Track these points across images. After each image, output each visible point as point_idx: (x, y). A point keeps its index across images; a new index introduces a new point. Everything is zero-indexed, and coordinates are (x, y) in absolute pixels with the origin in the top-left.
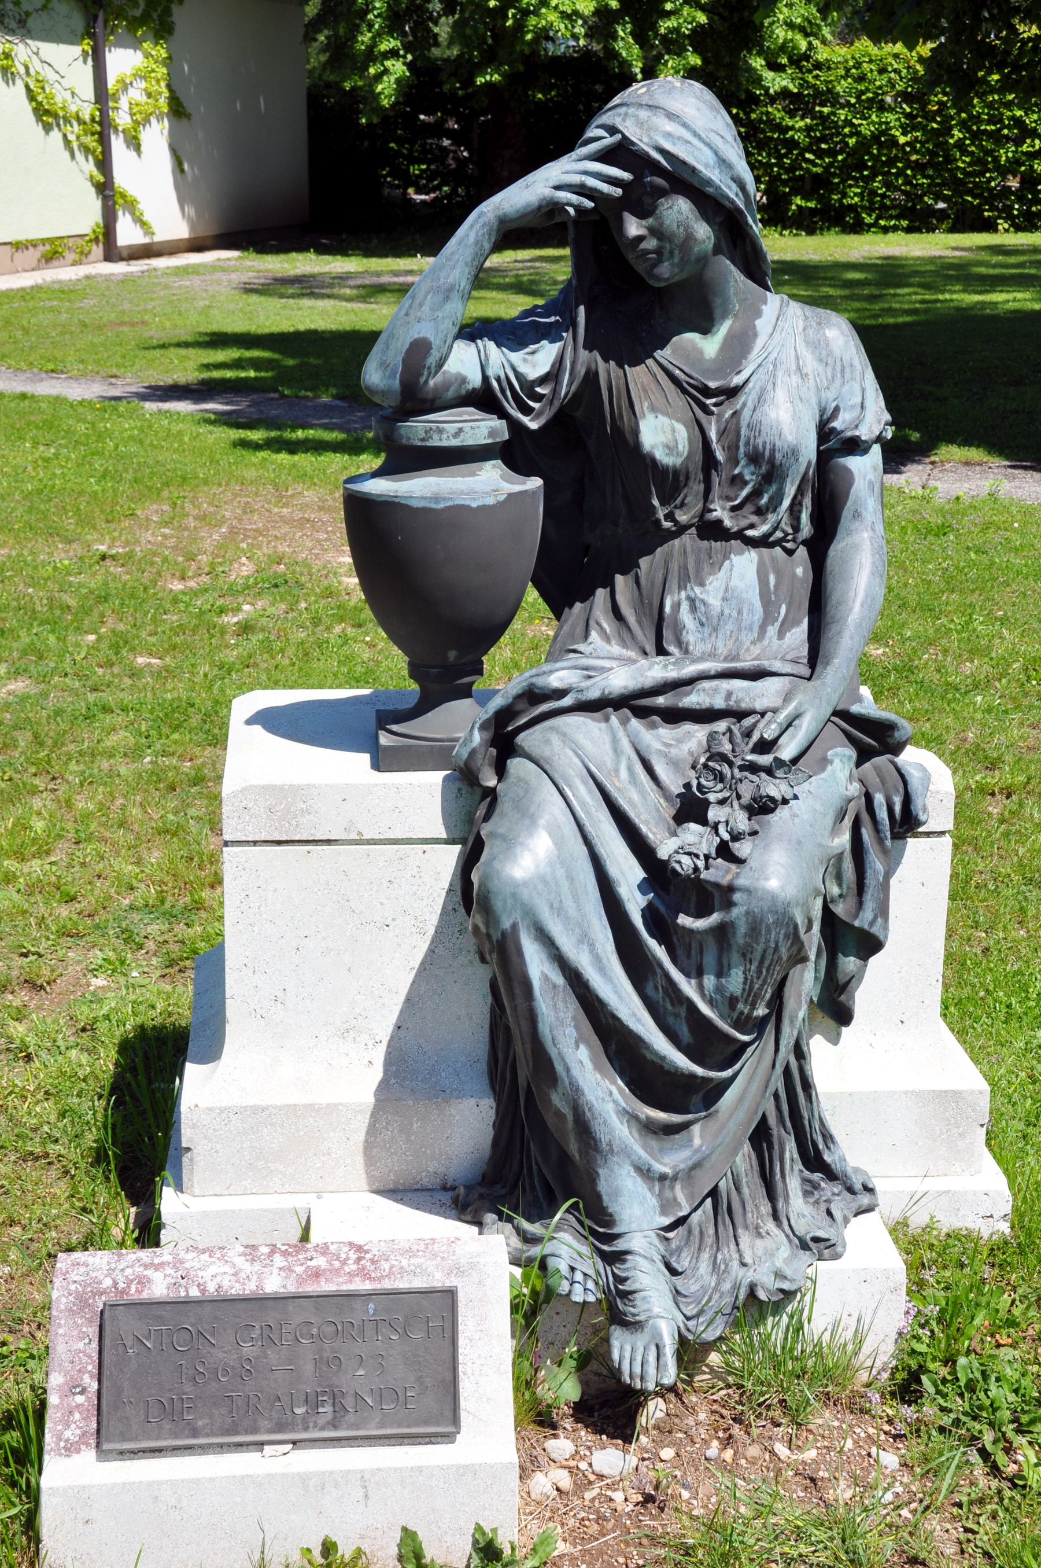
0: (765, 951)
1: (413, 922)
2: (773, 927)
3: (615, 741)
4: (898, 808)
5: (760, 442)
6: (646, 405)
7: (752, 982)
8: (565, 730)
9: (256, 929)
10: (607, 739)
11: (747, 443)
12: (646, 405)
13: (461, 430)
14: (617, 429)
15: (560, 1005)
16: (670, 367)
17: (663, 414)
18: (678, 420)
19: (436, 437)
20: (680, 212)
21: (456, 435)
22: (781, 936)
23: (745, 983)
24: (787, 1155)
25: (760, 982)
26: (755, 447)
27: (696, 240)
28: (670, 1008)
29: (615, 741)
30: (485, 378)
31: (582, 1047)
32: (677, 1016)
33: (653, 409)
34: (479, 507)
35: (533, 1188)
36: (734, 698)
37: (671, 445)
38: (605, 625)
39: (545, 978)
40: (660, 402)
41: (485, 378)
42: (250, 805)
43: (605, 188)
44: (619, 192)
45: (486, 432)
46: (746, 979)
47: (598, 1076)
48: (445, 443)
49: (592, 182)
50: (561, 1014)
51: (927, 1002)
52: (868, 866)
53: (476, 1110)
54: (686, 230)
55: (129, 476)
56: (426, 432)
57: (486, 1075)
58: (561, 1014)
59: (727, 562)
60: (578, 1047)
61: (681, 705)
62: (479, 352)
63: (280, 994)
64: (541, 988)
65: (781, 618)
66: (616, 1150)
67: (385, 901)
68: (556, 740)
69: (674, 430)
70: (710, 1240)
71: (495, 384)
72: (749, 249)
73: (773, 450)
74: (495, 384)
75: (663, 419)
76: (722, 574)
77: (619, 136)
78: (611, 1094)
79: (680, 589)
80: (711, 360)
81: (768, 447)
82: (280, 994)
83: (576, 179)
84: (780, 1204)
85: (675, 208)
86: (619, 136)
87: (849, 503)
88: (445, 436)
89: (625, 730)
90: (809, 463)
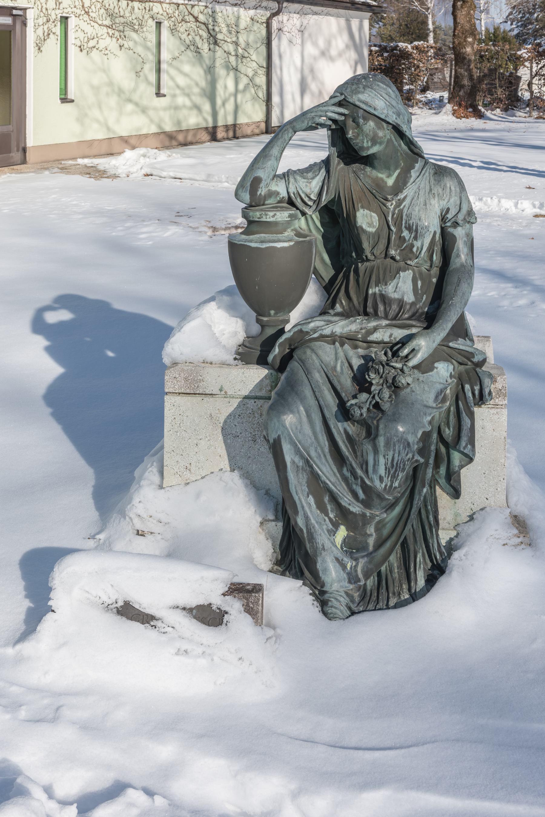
0: (394, 455)
1: (250, 435)
2: (397, 443)
3: (336, 354)
4: (477, 392)
5: (411, 222)
6: (360, 205)
7: (389, 469)
8: (314, 348)
9: (178, 434)
10: (333, 352)
11: (406, 223)
12: (360, 205)
13: (275, 214)
15: (301, 475)
16: (371, 190)
17: (367, 209)
18: (374, 212)
19: (264, 217)
20: (370, 126)
21: (273, 216)
22: (401, 448)
23: (386, 470)
24: (418, 560)
25: (394, 469)
26: (409, 225)
27: (378, 137)
28: (353, 480)
29: (336, 354)
31: (310, 496)
32: (357, 484)
33: (363, 207)
34: (281, 247)
35: (295, 568)
36: (393, 336)
37: (370, 223)
38: (343, 302)
39: (293, 462)
42: (177, 376)
44: (343, 118)
45: (287, 215)
46: (386, 468)
47: (319, 512)
48: (268, 220)
50: (301, 480)
51: (499, 489)
52: (462, 420)
53: (276, 528)
54: (373, 133)
56: (260, 215)
58: (301, 480)
59: (398, 275)
60: (308, 496)
61: (368, 339)
62: (286, 181)
63: (188, 466)
64: (291, 466)
65: (423, 301)
66: (326, 548)
67: (237, 424)
68: (309, 352)
69: (371, 216)
70: (374, 598)
71: (292, 195)
72: (408, 140)
75: (366, 212)
76: (395, 281)
78: (325, 520)
79: (376, 286)
82: (188, 466)
84: (413, 584)
85: (368, 124)
86: (343, 97)
87: (455, 251)
88: (268, 217)
89: (342, 349)
90: (435, 233)
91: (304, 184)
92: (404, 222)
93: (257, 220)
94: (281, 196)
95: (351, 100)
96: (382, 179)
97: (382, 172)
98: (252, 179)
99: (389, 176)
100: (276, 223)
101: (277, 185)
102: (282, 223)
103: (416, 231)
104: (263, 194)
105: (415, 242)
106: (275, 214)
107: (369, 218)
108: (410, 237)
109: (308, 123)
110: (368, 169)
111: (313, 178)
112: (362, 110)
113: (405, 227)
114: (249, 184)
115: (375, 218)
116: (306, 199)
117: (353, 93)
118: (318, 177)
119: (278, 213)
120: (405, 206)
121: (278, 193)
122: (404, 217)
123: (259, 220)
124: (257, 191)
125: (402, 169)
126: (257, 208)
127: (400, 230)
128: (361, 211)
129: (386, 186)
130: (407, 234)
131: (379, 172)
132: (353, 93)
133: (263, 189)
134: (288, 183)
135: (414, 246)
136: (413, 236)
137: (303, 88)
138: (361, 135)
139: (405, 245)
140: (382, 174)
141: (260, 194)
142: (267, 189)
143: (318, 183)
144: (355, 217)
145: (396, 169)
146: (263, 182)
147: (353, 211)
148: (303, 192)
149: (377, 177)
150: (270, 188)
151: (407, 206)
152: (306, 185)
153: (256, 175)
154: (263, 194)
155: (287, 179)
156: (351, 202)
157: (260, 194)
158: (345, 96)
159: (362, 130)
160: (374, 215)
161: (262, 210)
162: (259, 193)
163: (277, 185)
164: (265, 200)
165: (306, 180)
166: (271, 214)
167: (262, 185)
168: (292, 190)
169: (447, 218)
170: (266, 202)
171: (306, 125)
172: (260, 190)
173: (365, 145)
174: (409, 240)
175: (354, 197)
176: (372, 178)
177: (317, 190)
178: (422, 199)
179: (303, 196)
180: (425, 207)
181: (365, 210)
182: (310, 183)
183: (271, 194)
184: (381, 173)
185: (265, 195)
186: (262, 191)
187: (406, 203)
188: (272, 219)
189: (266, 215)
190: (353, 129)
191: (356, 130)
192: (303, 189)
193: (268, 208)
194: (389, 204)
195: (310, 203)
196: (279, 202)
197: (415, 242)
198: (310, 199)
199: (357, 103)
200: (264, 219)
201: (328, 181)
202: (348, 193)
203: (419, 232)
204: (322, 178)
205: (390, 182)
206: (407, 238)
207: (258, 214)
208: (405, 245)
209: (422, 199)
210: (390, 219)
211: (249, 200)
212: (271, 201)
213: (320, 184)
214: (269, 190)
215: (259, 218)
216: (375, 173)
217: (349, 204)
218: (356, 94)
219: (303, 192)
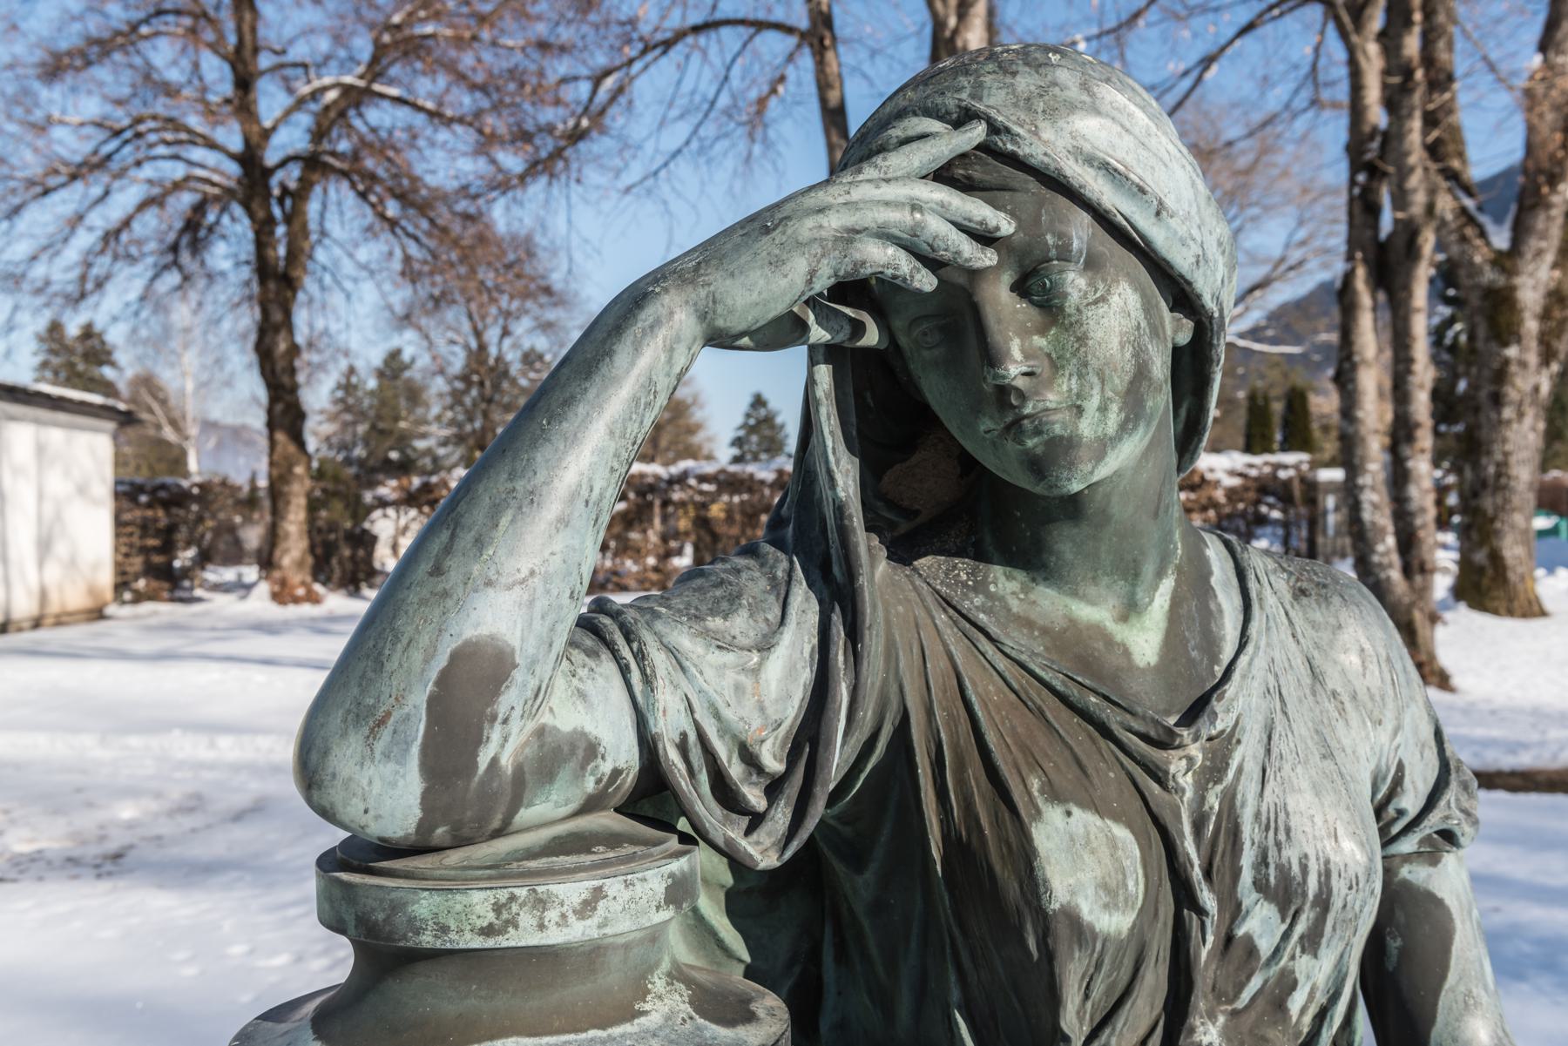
5: (1291, 855)
6: (1035, 784)
11: (1262, 861)
12: (1035, 784)
13: (598, 894)
14: (961, 850)
16: (1074, 692)
17: (1082, 805)
18: (1116, 818)
19: (527, 919)
21: (587, 908)
26: (1284, 871)
30: (648, 745)
33: (1055, 795)
40: (1066, 777)
41: (648, 745)
43: (969, 251)
49: (936, 227)
54: (1136, 355)
55: (777, 252)
56: (498, 908)
57: (295, 773)
62: (624, 671)
69: (1113, 843)
71: (673, 755)
73: (1326, 875)
74: (673, 755)
77: (976, 133)
80: (1148, 669)
81: (1314, 868)
83: (899, 218)
86: (976, 133)
88: (552, 915)
91: (731, 677)
92: (1247, 859)
93: (477, 943)
94: (606, 768)
95: (1031, 149)
96: (1099, 631)
97: (1092, 590)
98: (441, 661)
99: (1130, 610)
100: (591, 955)
101: (582, 695)
102: (627, 947)
103: (1323, 903)
104: (507, 762)
105: (1303, 965)
106: (598, 894)
107: (1104, 852)
108: (1286, 936)
109: (812, 274)
110: (1004, 582)
111: (765, 646)
112: (1085, 218)
113: (1260, 885)
114: (418, 700)
115: (1124, 845)
116: (735, 770)
117: (1030, 109)
118: (788, 636)
119: (614, 886)
120: (1240, 770)
121: (592, 750)
122: (1248, 831)
123: (490, 943)
124: (478, 740)
125: (1179, 570)
126: (454, 857)
127: (1234, 911)
128: (1053, 814)
129: (1131, 667)
130: (1265, 921)
131: (1074, 594)
132: (1030, 109)
133: (515, 725)
134: (648, 680)
135: (1293, 985)
136: (1300, 928)
137: (44, 547)
138: (1071, 368)
139: (1255, 983)
140: (1093, 603)
141: (494, 761)
142: (531, 726)
143: (791, 672)
144: (1025, 857)
145: (1160, 574)
146: (518, 675)
147: (997, 822)
148: (724, 729)
149: (1073, 622)
150: (545, 718)
151: (1252, 768)
152: (738, 689)
153: (469, 633)
154: (507, 762)
155: (626, 652)
156: (975, 772)
157: (494, 761)
158: (994, 129)
159: (1082, 339)
160: (1122, 833)
161: (499, 871)
162: (483, 760)
163: (582, 695)
164: (516, 804)
165: (730, 658)
166: (572, 891)
167: (511, 699)
168: (669, 723)
169: (1401, 813)
170: (524, 815)
171: (800, 283)
172: (495, 735)
173: (1087, 428)
174: (1277, 952)
175: (991, 738)
176: (1045, 631)
177: (791, 710)
178: (1302, 728)
179: (722, 749)
180: (1328, 764)
181: (1076, 810)
182: (756, 672)
183: (558, 755)
184: (1084, 598)
185: (519, 771)
186: (504, 746)
187: (1246, 754)
188: (578, 931)
189: (541, 904)
190: (1024, 333)
191: (1039, 341)
192: (728, 714)
193: (531, 854)
194: (1176, 765)
195: (754, 797)
196: (591, 805)
197: (1303, 965)
198: (750, 759)
199: (1076, 172)
200: (525, 936)
201: (856, 657)
202: (952, 720)
203: (1337, 903)
204: (810, 641)
205: (1144, 641)
206: (1265, 946)
207: (480, 903)
208: (1255, 983)
209: (1302, 728)
210: (1189, 846)
211: (417, 813)
212: (548, 809)
213: (806, 675)
214: (541, 732)
215: (488, 931)
216: (1050, 603)
217: (961, 782)
218: (1051, 113)
219: (724, 729)
